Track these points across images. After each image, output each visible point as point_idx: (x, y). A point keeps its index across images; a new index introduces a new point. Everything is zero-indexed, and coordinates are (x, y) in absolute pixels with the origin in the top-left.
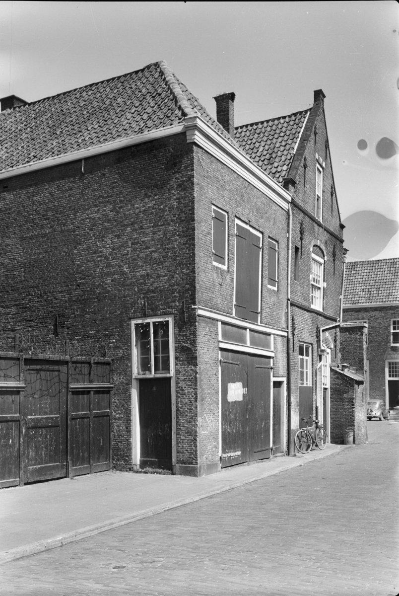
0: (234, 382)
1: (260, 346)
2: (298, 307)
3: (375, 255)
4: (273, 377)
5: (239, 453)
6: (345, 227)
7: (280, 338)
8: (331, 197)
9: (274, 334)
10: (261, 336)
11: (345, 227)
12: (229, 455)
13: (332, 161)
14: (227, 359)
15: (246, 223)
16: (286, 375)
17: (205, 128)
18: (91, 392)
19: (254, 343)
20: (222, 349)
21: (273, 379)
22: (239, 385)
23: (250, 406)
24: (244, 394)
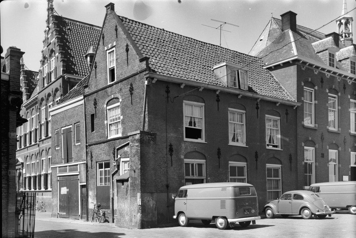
0: (63, 187)
1: (74, 171)
2: (95, 145)
3: (142, 20)
4: (80, 183)
5: (65, 213)
6: (297, 14)
7: (83, 165)
8: (126, 54)
9: (79, 164)
10: (74, 167)
11: (297, 14)
12: (61, 213)
13: (337, 18)
14: (61, 179)
15: (66, 126)
16: (85, 181)
17: (79, 98)
18: (183, 84)
19: (71, 171)
20: (59, 176)
21: (80, 184)
22: (65, 188)
23: (70, 196)
24: (67, 192)
